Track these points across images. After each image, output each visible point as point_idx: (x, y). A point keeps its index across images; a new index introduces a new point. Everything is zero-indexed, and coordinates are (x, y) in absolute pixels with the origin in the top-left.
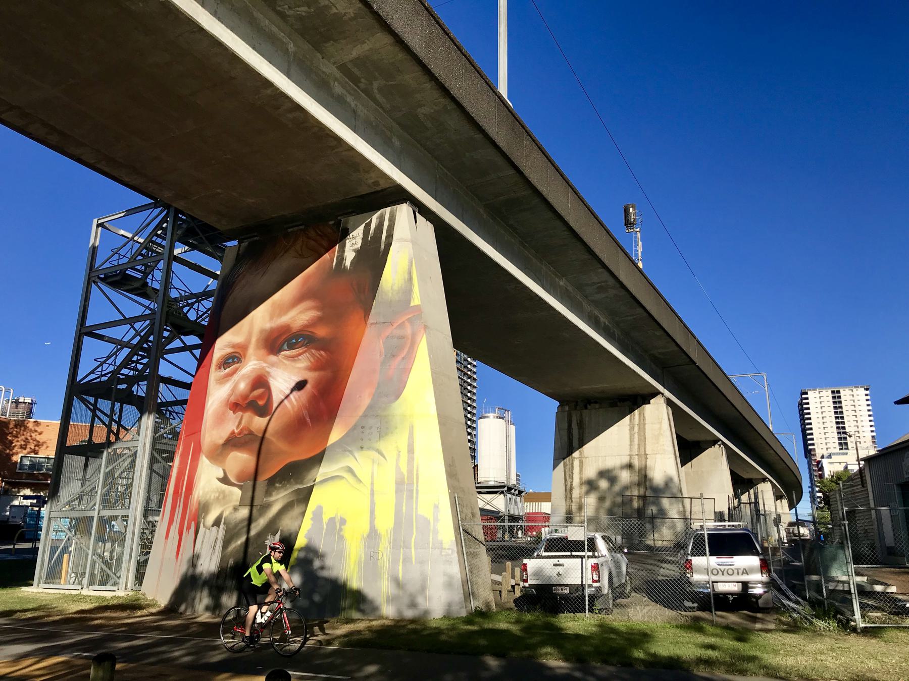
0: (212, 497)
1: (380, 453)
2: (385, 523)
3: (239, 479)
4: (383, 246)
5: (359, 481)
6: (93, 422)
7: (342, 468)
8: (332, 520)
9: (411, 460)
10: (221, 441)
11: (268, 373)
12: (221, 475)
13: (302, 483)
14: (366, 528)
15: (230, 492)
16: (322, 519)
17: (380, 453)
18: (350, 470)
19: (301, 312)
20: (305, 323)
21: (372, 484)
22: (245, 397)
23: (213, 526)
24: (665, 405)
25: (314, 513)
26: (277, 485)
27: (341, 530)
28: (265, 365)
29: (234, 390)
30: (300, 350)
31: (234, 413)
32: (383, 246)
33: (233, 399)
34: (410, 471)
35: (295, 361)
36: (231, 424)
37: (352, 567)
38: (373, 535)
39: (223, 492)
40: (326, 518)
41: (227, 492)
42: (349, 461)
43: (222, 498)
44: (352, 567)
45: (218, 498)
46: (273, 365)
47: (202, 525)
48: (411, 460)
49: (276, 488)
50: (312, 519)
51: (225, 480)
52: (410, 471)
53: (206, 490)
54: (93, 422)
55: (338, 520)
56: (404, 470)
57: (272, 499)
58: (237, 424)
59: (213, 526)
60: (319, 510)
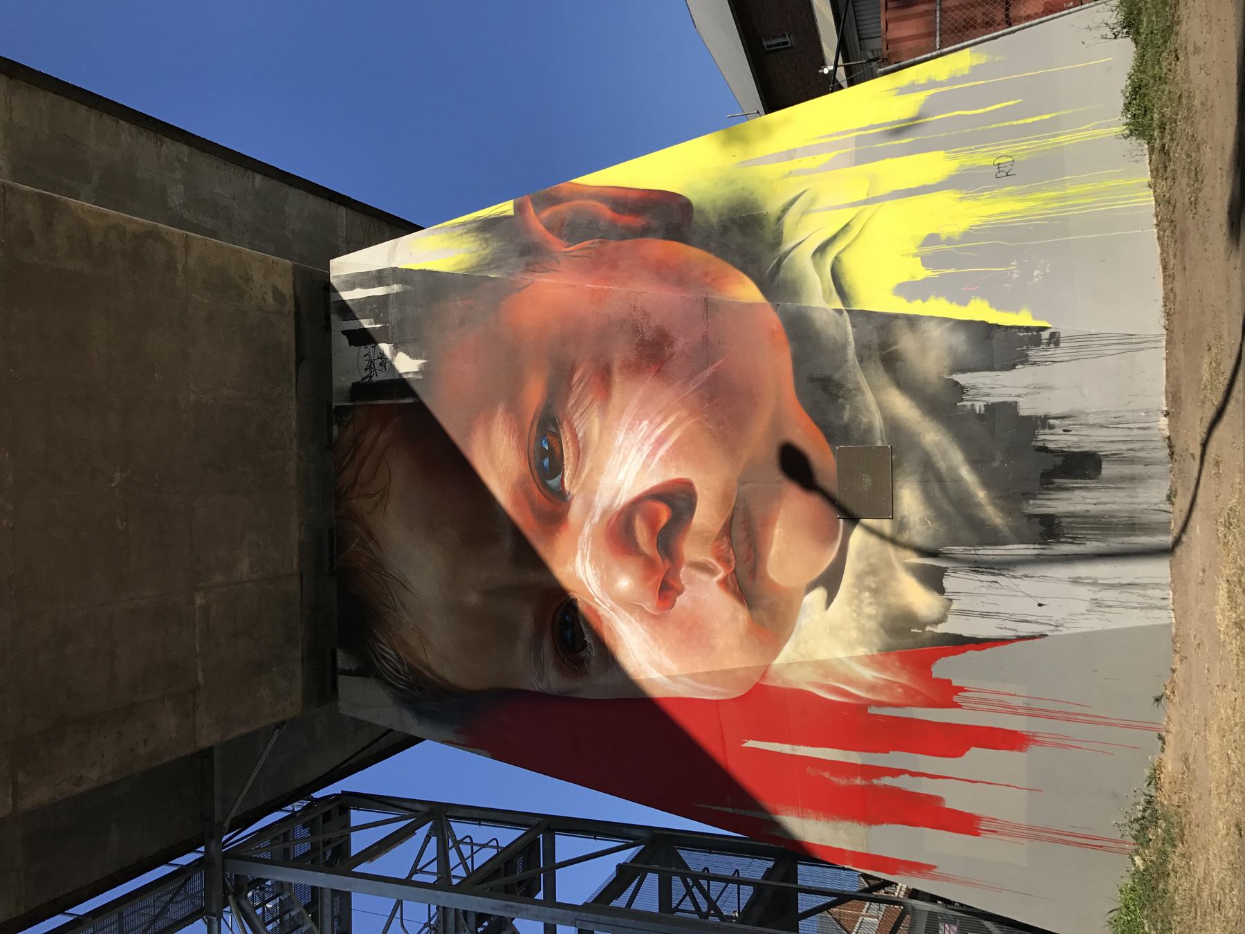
0: (870, 610)
1: (785, 210)
2: (934, 165)
3: (826, 537)
4: (396, 288)
5: (845, 229)
6: (684, 897)
7: (817, 266)
8: (927, 262)
9: (809, 151)
10: (743, 615)
11: (605, 513)
12: (819, 594)
13: (844, 347)
14: (946, 198)
15: (859, 554)
16: (926, 280)
17: (785, 210)
18: (822, 249)
19: (492, 462)
20: (514, 443)
21: (854, 204)
22: (650, 564)
23: (941, 590)
24: (681, 600)
25: (910, 298)
26: (846, 415)
27: (950, 240)
28: (587, 529)
29: (630, 606)
30: (566, 437)
31: (679, 592)
32: (396, 288)
33: (650, 605)
34: (830, 147)
35: (585, 447)
36: (705, 593)
37: (1032, 204)
38: (962, 182)
39: (860, 577)
40: (922, 273)
41: (861, 566)
42: (802, 259)
43: (876, 581)
44: (1032, 204)
45: (875, 592)
46: (588, 506)
47: (941, 629)
48: (809, 151)
49: (854, 418)
50: (924, 300)
51: (830, 581)
52: (830, 147)
53: (854, 634)
54: (684, 897)
55: (928, 250)
56: (825, 158)
57: (878, 422)
58: (704, 577)
59: (941, 590)
60: (908, 290)
